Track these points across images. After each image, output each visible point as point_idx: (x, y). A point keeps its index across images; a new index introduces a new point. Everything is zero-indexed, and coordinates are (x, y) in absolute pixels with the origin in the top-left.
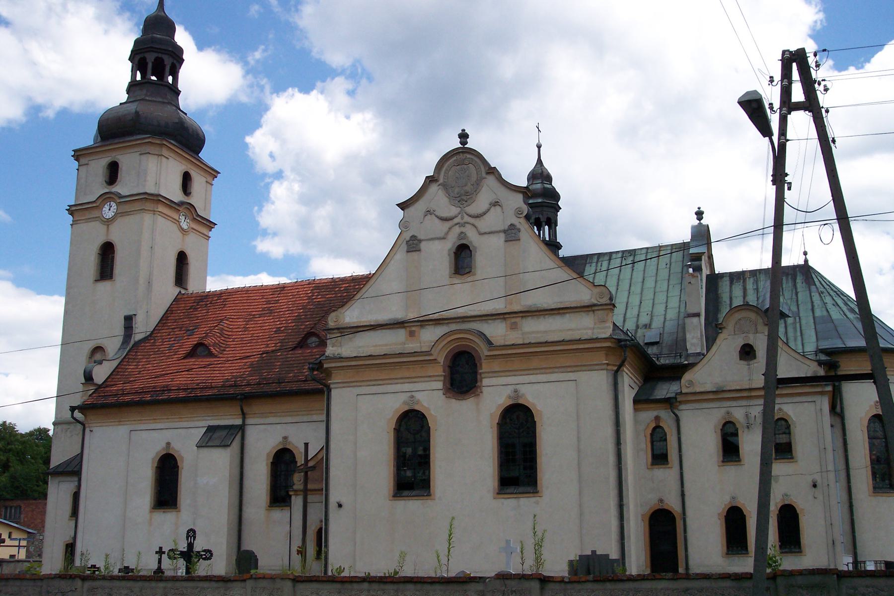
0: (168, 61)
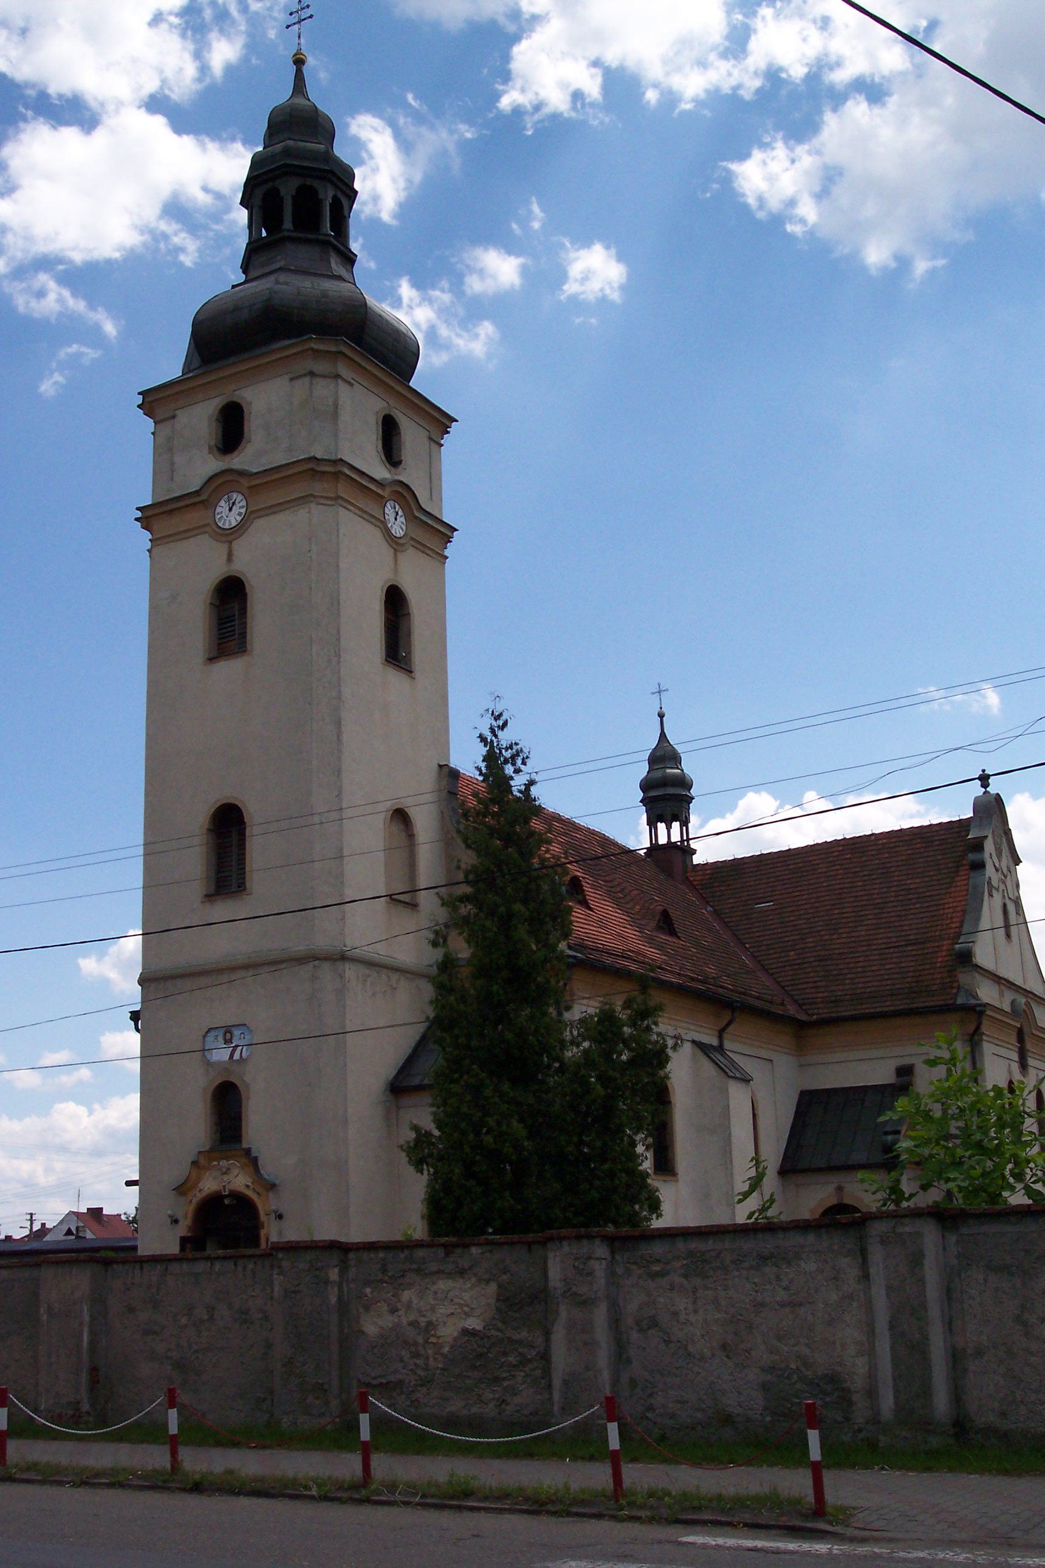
0: (327, 195)
